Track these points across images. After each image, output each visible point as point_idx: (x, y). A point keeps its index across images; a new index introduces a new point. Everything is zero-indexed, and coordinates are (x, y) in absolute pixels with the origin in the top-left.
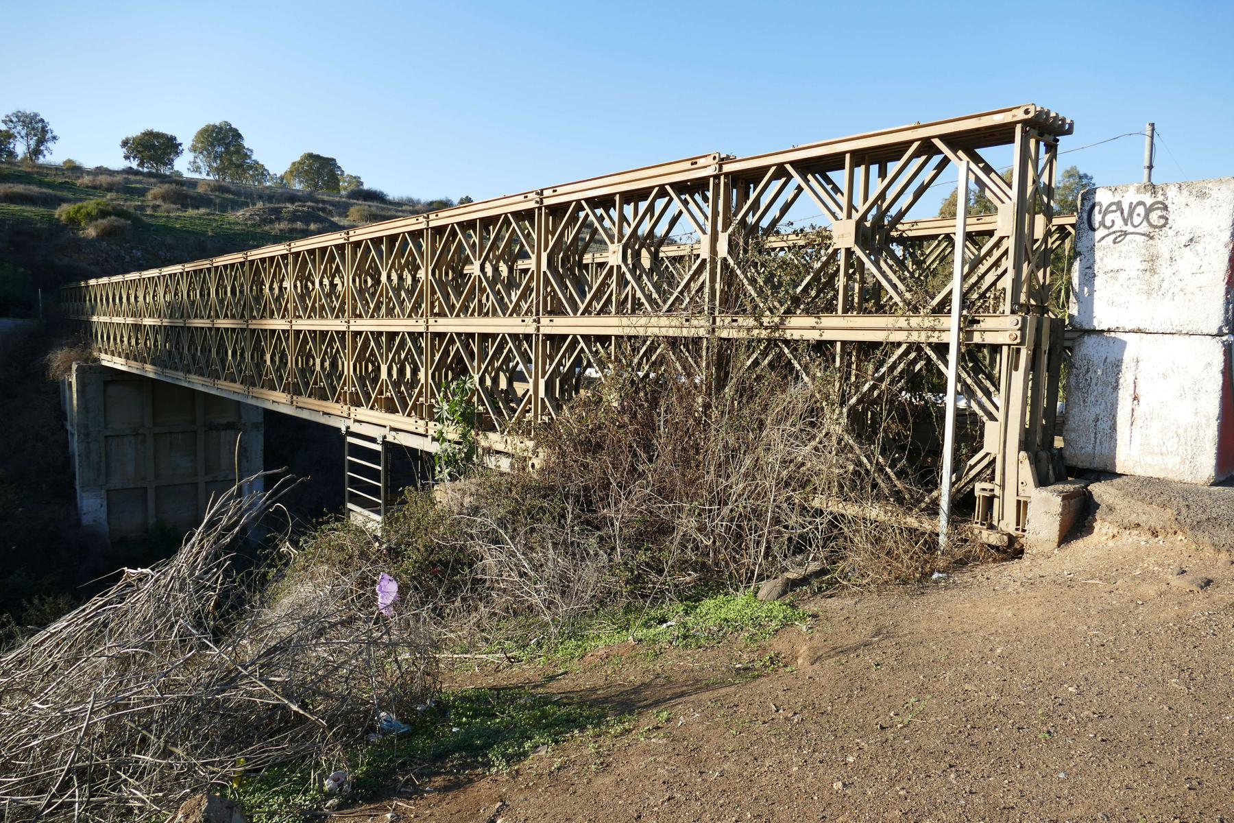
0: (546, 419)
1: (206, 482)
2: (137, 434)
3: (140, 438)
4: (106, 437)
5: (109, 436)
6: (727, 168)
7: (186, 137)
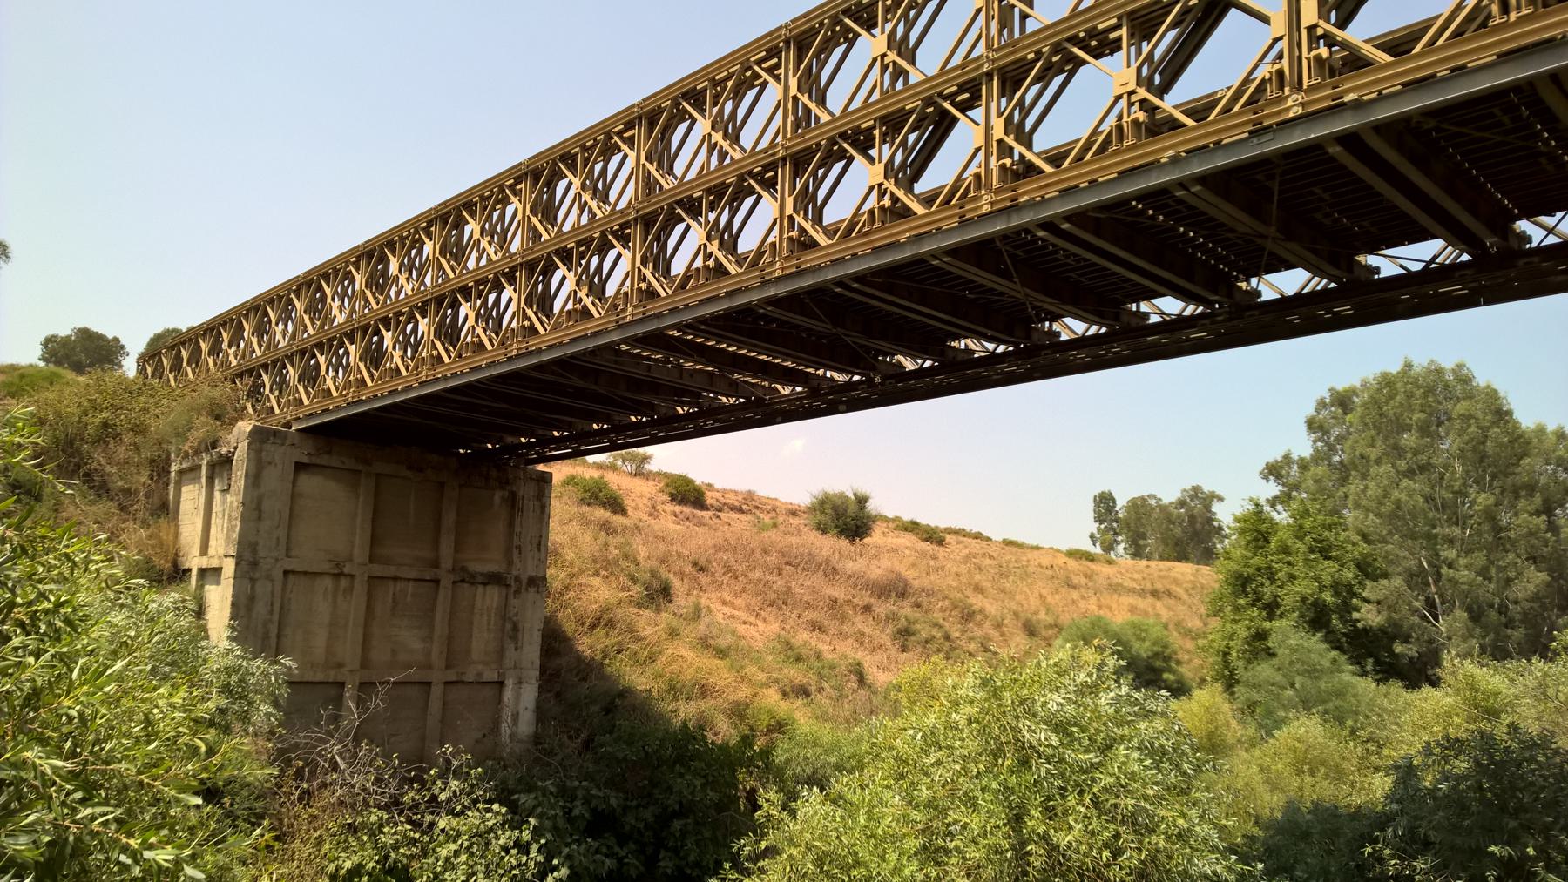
0: (526, 323)
1: (446, 683)
2: (341, 574)
3: (344, 582)
4: (286, 573)
5: (293, 572)
6: (790, 151)
7: (135, 345)
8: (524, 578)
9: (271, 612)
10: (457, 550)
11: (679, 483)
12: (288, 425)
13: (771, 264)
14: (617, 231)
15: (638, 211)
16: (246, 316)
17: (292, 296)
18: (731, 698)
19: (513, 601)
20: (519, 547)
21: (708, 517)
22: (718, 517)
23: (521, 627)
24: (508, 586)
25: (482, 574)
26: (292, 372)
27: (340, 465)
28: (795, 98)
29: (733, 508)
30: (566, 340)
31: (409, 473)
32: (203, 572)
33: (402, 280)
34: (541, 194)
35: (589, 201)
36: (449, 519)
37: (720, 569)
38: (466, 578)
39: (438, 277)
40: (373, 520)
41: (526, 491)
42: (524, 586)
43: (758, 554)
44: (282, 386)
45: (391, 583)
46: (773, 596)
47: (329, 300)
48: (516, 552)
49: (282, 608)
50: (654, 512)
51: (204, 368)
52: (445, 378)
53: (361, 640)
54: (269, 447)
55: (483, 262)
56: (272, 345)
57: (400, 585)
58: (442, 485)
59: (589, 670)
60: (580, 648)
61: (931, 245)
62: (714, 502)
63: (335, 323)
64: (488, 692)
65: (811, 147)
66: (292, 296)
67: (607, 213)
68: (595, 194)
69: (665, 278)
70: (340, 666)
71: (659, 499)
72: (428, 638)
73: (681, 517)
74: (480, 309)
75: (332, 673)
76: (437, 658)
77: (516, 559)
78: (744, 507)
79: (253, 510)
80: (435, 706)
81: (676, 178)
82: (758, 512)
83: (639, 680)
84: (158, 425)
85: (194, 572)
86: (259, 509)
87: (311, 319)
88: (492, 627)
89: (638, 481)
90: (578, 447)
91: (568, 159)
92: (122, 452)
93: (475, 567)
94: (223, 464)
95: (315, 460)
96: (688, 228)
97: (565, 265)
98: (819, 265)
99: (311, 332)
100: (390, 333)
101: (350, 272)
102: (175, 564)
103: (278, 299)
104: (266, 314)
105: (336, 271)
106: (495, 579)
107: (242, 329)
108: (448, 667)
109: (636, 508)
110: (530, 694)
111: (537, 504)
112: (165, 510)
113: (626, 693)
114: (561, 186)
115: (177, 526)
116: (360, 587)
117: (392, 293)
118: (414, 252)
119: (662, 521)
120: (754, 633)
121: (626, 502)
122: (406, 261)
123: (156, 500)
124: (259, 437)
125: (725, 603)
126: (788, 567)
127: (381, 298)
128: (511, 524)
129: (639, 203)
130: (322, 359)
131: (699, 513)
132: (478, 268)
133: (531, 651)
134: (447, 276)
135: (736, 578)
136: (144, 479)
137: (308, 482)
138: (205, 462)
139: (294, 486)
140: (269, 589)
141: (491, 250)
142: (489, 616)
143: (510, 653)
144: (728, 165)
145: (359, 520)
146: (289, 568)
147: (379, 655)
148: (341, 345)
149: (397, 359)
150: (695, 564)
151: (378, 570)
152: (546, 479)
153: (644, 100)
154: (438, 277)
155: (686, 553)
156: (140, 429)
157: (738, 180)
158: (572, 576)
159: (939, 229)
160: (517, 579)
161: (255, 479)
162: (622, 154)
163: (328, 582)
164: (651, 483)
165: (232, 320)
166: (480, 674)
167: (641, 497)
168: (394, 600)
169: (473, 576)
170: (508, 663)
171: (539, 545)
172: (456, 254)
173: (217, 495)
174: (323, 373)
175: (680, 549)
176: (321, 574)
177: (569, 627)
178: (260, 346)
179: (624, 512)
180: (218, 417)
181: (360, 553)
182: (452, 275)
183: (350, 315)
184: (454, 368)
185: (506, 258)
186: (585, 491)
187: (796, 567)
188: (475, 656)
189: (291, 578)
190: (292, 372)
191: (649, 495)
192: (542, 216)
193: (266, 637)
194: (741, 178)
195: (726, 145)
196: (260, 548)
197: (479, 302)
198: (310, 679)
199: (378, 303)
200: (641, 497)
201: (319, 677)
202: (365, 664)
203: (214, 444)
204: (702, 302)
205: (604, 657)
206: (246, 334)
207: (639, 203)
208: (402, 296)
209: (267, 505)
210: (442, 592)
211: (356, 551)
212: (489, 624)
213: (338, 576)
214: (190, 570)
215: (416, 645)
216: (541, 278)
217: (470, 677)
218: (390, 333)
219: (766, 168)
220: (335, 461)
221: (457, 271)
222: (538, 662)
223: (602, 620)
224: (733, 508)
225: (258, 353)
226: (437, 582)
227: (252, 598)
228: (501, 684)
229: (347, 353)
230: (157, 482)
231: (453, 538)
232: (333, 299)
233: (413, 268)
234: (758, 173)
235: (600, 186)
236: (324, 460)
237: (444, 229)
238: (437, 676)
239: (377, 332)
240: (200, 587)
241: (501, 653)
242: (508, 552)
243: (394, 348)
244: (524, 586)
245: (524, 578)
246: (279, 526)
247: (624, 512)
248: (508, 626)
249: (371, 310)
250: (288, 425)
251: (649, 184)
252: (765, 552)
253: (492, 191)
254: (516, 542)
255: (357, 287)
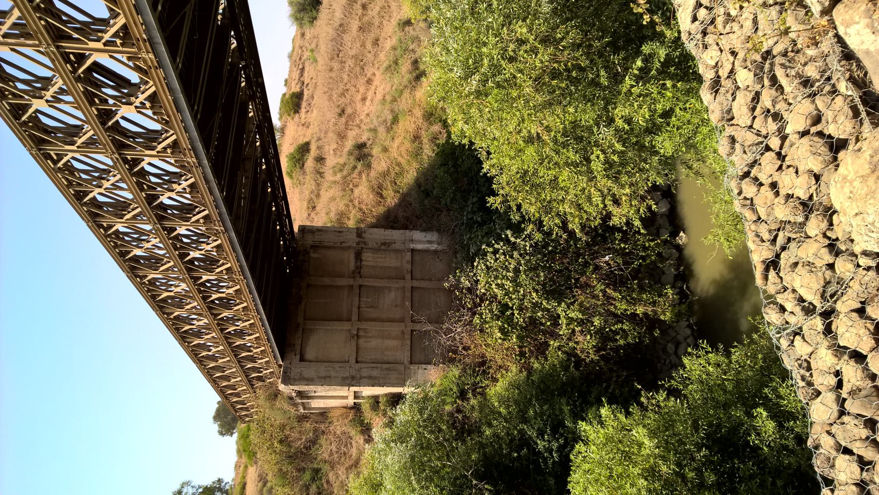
1: (412, 279)
3: (361, 333)
4: (357, 362)
5: (357, 358)
8: (358, 240)
9: (377, 368)
10: (342, 276)
11: (287, 108)
12: (280, 366)
13: (145, 61)
14: (129, 165)
15: (155, 223)
16: (169, 314)
17: (172, 317)
18: (421, 121)
19: (370, 245)
20: (341, 243)
21: (308, 92)
22: (307, 85)
23: (383, 241)
24: (362, 248)
25: (356, 262)
26: (226, 314)
27: (300, 339)
28: (78, 147)
29: (302, 75)
30: (234, 255)
31: (303, 304)
32: (355, 397)
33: (148, 245)
34: (108, 212)
35: (110, 182)
36: (327, 281)
37: (343, 100)
38: (358, 271)
39: (142, 220)
40: (329, 320)
41: (310, 240)
42: (361, 240)
43: (333, 75)
44: (232, 320)
45: (361, 309)
46: (358, 69)
47: (172, 294)
48: (344, 245)
49: (374, 363)
50: (306, 125)
51: (227, 364)
52: (256, 305)
53: (389, 323)
54: (292, 375)
55: (124, 185)
56: (207, 327)
57: (362, 305)
58: (309, 286)
59: (404, 200)
60: (393, 204)
61: (172, 77)
62: (298, 86)
63: (188, 289)
64: (417, 257)
65: (110, 140)
66: (172, 317)
67: (90, 128)
68: (104, 179)
69: (162, 134)
70: (403, 332)
71: (298, 120)
72: (389, 289)
73: (308, 108)
74: (164, 188)
75: (406, 336)
76: (401, 283)
77: (347, 245)
78: (301, 67)
79: (326, 380)
80: (423, 284)
81: (54, 76)
82: (303, 59)
83: (410, 176)
84: (279, 420)
85: (356, 401)
86: (325, 378)
87: (187, 304)
88: (383, 256)
89: (287, 132)
90: (285, 215)
91: (80, 195)
92: (295, 435)
93: (352, 266)
94: (300, 394)
95: (298, 352)
96: (123, 118)
97: (140, 163)
98: (189, 139)
99: (195, 304)
100: (191, 253)
101: (148, 281)
102: (351, 408)
103: (194, 353)
104: (186, 332)
105: (149, 290)
106: (358, 256)
107: (198, 345)
108: (404, 279)
109: (304, 136)
110: (417, 235)
111: (317, 234)
112: (324, 414)
113: (417, 180)
114: (101, 199)
115: (332, 408)
116: (364, 325)
117: (161, 252)
118: (126, 238)
119: (312, 120)
120: (382, 88)
121: (301, 142)
122: (135, 244)
123: (320, 418)
124: (286, 380)
125: (364, 99)
126: (340, 55)
127: (165, 260)
128: (328, 247)
129: (107, 151)
130: (214, 296)
131: (305, 97)
132: (129, 190)
133: (396, 235)
134: (140, 212)
135: (348, 90)
136: (308, 425)
137: (310, 354)
138: (300, 401)
139: (311, 361)
140: (365, 370)
141: (113, 180)
142: (378, 258)
143: (398, 246)
144: (67, 86)
145: (329, 328)
146: (354, 361)
147: (397, 313)
148: (203, 284)
149: (208, 248)
150: (340, 115)
151: (355, 317)
152: (303, 229)
153: (83, 219)
154: (142, 220)
155: (333, 120)
156: (283, 427)
157: (80, 82)
158: (355, 207)
159: (165, 79)
160: (358, 243)
161: (309, 381)
162: (71, 160)
163: (361, 341)
164: (288, 124)
165: (174, 324)
166: (408, 262)
167: (297, 131)
168: (370, 307)
169: (357, 267)
170: (402, 247)
171: (340, 232)
172: (156, 260)
173: (316, 394)
174: (223, 295)
175: (331, 124)
176: (357, 344)
177: (381, 210)
178: (209, 334)
179: (307, 144)
180: (276, 396)
181: (346, 326)
182: (139, 210)
183: (181, 280)
184: (232, 261)
185: (117, 166)
186: (296, 166)
187: (340, 51)
188: (398, 264)
189: (359, 359)
190: (226, 314)
191: (296, 126)
192: (125, 211)
193: (389, 369)
194: (78, 79)
195: (53, 90)
196: (345, 376)
197: (159, 189)
198: (409, 347)
199: (169, 262)
200: (297, 131)
201: (409, 342)
202: (402, 320)
203: (291, 398)
204: (211, 193)
205: (399, 192)
206: (202, 342)
207: (107, 151)
208: (161, 245)
209: (323, 374)
210: (365, 283)
211: (345, 328)
212: (382, 258)
213: (358, 336)
214: (355, 403)
215: (393, 294)
216: (169, 211)
217: (409, 267)
218: (191, 253)
219: (67, 60)
220: (298, 342)
221: (136, 205)
222: (402, 231)
223: (379, 191)
224: (302, 75)
225: (214, 334)
226: (360, 286)
227: (370, 377)
228: (413, 250)
229: (208, 281)
230: (310, 419)
231: (337, 279)
232: (171, 291)
233: (140, 237)
234: (72, 66)
235: (96, 174)
236: (298, 348)
237: (103, 216)
238: (409, 284)
239: (191, 262)
240: (363, 398)
241: (397, 251)
242: (344, 249)
243: (201, 250)
244: (361, 240)
245: (358, 240)
246: (334, 368)
247: (307, 144)
248: (383, 247)
249: (122, 180)
250: (280, 366)
251: (91, 143)
252: (331, 70)
253: (110, 242)
254: (338, 245)
255: (160, 276)
